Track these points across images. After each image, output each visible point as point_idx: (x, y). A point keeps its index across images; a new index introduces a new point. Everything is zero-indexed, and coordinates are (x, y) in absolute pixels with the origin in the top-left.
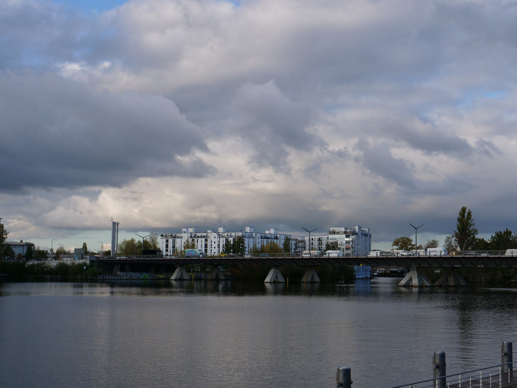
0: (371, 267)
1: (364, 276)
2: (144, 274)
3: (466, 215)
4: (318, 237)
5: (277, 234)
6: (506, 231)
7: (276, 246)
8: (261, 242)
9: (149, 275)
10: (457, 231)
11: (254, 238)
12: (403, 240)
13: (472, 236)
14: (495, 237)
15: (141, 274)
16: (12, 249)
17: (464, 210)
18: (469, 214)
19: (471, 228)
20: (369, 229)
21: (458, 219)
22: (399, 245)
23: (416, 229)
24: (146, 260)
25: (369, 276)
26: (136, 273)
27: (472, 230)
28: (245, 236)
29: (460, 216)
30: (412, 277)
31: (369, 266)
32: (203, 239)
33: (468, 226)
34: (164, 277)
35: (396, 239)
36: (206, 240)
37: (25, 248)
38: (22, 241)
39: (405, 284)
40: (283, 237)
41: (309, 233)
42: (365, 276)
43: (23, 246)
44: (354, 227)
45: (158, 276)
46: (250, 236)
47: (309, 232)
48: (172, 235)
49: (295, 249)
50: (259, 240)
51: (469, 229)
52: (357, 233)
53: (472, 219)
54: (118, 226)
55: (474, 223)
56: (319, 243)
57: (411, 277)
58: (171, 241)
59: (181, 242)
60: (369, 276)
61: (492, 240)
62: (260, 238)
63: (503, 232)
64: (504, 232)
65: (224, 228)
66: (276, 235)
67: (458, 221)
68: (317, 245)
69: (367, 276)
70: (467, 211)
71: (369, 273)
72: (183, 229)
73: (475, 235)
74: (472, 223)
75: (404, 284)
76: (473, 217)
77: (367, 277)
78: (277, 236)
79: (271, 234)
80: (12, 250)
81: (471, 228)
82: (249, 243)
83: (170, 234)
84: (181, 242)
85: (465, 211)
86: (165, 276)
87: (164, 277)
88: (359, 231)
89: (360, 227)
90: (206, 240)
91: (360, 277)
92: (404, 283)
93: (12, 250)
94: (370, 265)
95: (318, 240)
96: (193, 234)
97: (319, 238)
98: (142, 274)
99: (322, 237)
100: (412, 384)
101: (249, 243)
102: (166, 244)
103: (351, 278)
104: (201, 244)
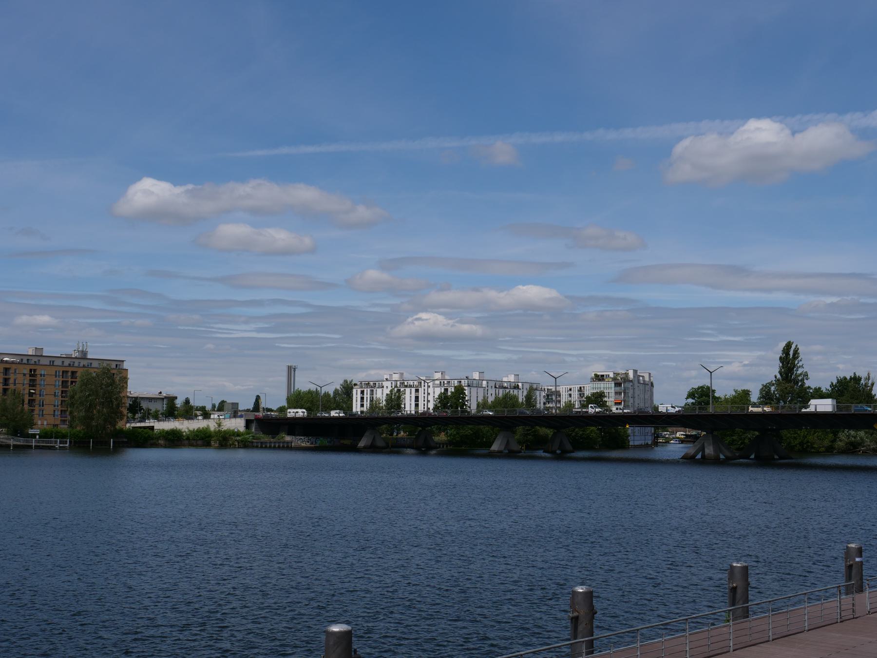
0: (653, 429)
1: (643, 442)
2: (322, 439)
3: (791, 353)
4: (579, 386)
5: (518, 382)
6: (852, 377)
7: (515, 398)
8: (496, 393)
9: (329, 440)
10: (779, 376)
11: (485, 387)
12: (703, 390)
13: (800, 384)
14: (836, 385)
15: (317, 438)
16: (140, 405)
17: (789, 345)
18: (796, 352)
19: (799, 372)
20: (650, 374)
21: (781, 358)
22: (696, 397)
23: (711, 373)
24: (350, 418)
25: (650, 443)
26: (310, 438)
27: (801, 374)
28: (473, 384)
29: (783, 355)
30: (705, 444)
31: (649, 428)
32: (413, 390)
33: (795, 369)
34: (350, 444)
35: (692, 388)
36: (417, 391)
37: (165, 403)
38: (161, 393)
39: (694, 454)
40: (527, 386)
41: (557, 379)
42: (643, 442)
43: (163, 399)
44: (628, 371)
45: (342, 441)
46: (478, 384)
47: (711, 374)
48: (368, 383)
49: (544, 404)
50: (492, 391)
51: (796, 373)
52: (631, 379)
53: (799, 359)
54: (294, 371)
55: (803, 364)
56: (580, 394)
57: (703, 445)
58: (367, 391)
59: (382, 393)
60: (650, 443)
61: (832, 389)
62: (493, 387)
63: (848, 378)
64: (851, 376)
65: (442, 374)
66: (517, 384)
67: (780, 362)
68: (576, 398)
69: (646, 441)
70: (793, 347)
71: (650, 438)
72: (385, 375)
73: (805, 381)
74: (800, 364)
75: (692, 454)
76: (801, 356)
77: (647, 443)
78: (518, 385)
79: (510, 382)
80: (141, 405)
81: (799, 372)
82: (477, 394)
83: (576, 386)
84: (382, 393)
85: (791, 347)
86: (352, 441)
87: (350, 444)
88: (634, 377)
89: (635, 372)
90: (417, 391)
91: (637, 443)
92: (693, 452)
93: (141, 405)
94: (651, 427)
95: (579, 391)
96: (398, 383)
97: (581, 388)
98: (319, 438)
99: (583, 386)
100: (854, 618)
101: (477, 394)
102: (3, 388)
103: (620, 443)
104: (358, 396)
